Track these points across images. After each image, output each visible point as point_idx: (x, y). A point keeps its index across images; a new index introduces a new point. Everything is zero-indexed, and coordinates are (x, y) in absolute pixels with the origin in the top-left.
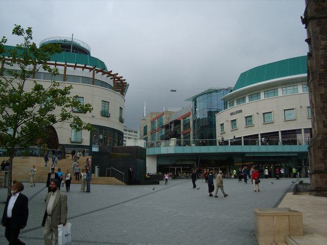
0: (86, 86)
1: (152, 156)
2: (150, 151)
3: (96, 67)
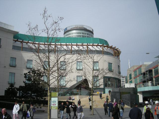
0: (19, 52)
1: (140, 92)
2: (139, 90)
3: (104, 44)
